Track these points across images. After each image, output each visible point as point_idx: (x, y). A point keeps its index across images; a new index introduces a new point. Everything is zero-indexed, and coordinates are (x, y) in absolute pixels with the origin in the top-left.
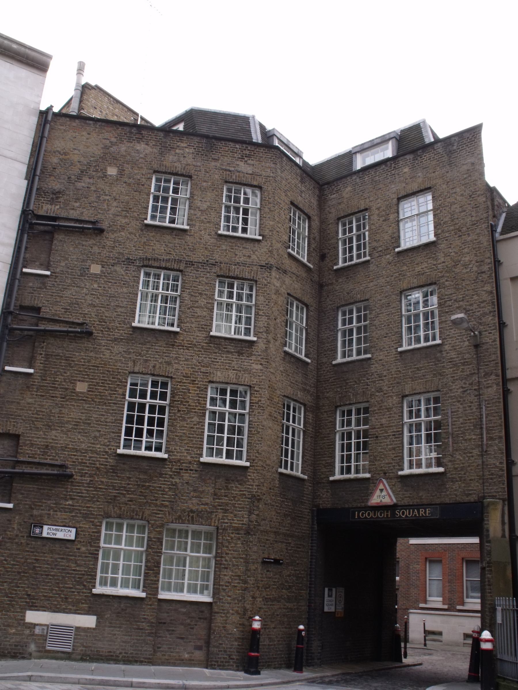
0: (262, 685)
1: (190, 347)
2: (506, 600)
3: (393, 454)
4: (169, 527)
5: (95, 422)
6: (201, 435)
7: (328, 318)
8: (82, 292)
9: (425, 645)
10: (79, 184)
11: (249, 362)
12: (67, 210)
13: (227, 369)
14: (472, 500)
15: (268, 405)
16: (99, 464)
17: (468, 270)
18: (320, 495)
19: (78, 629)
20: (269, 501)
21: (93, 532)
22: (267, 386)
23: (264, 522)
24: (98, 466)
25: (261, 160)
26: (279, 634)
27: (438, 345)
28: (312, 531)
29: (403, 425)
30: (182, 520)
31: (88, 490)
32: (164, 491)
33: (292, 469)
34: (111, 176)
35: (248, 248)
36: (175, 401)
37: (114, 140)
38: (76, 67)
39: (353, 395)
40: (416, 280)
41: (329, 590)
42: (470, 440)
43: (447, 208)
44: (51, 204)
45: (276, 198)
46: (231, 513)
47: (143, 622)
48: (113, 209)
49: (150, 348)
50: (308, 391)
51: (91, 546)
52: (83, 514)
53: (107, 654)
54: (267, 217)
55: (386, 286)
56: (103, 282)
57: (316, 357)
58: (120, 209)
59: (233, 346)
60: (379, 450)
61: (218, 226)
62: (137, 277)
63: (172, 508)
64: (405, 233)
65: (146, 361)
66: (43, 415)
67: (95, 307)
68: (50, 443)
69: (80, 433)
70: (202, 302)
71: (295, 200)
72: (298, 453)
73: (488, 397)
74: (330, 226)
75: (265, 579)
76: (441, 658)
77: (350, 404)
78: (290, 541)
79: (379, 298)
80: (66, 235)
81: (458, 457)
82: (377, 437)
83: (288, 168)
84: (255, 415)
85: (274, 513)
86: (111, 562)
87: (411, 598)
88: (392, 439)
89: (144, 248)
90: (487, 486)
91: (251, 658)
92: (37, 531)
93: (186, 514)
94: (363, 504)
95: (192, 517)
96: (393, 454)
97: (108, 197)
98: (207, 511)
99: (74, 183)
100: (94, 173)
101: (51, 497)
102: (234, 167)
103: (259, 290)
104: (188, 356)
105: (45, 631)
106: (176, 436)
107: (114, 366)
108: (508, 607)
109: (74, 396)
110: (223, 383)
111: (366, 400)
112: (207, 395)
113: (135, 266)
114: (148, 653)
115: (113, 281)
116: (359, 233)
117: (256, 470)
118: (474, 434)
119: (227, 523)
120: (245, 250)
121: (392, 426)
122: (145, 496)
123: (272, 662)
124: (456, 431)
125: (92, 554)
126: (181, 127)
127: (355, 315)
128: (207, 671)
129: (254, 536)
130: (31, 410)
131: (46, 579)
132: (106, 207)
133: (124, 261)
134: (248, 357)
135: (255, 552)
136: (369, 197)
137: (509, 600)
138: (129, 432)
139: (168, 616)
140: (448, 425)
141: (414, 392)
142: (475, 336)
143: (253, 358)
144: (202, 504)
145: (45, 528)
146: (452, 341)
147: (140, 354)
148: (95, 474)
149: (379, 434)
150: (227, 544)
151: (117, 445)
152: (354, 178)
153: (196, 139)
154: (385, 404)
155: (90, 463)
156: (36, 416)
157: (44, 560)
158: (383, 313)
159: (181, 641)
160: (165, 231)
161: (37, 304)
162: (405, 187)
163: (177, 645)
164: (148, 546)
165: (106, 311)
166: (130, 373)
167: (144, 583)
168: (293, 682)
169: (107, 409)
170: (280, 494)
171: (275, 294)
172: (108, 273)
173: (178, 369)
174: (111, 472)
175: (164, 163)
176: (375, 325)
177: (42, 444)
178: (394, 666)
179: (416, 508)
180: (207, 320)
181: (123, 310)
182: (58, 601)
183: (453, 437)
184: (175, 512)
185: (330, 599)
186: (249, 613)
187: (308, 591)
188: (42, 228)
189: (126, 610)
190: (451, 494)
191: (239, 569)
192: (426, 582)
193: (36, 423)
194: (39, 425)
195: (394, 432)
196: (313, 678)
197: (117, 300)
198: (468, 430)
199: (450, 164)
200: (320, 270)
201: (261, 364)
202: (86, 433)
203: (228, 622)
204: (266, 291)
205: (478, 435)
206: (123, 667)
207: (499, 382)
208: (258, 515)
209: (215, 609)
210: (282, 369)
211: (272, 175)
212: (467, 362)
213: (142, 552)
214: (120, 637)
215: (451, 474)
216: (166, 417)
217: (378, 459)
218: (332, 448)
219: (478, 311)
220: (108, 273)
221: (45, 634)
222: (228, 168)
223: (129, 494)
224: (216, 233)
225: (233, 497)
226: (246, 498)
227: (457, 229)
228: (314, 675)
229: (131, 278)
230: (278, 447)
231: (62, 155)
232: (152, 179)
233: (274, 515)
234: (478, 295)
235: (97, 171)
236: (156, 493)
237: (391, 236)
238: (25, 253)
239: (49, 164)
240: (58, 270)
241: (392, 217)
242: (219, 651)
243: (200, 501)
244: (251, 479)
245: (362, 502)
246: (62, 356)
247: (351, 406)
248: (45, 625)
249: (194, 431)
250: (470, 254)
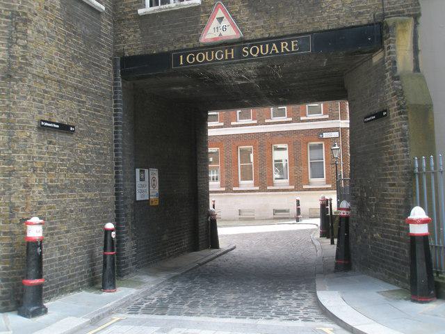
14: (365, 22)
18: (124, 37)
28: (115, 89)
78: (84, 99)
85: (55, 50)
94: (192, 44)
123: (67, 283)
129: (20, 83)
179: (274, 42)
185: (142, 183)
190: (329, 17)
208: (25, 47)
233: (56, 54)
245: (190, 41)
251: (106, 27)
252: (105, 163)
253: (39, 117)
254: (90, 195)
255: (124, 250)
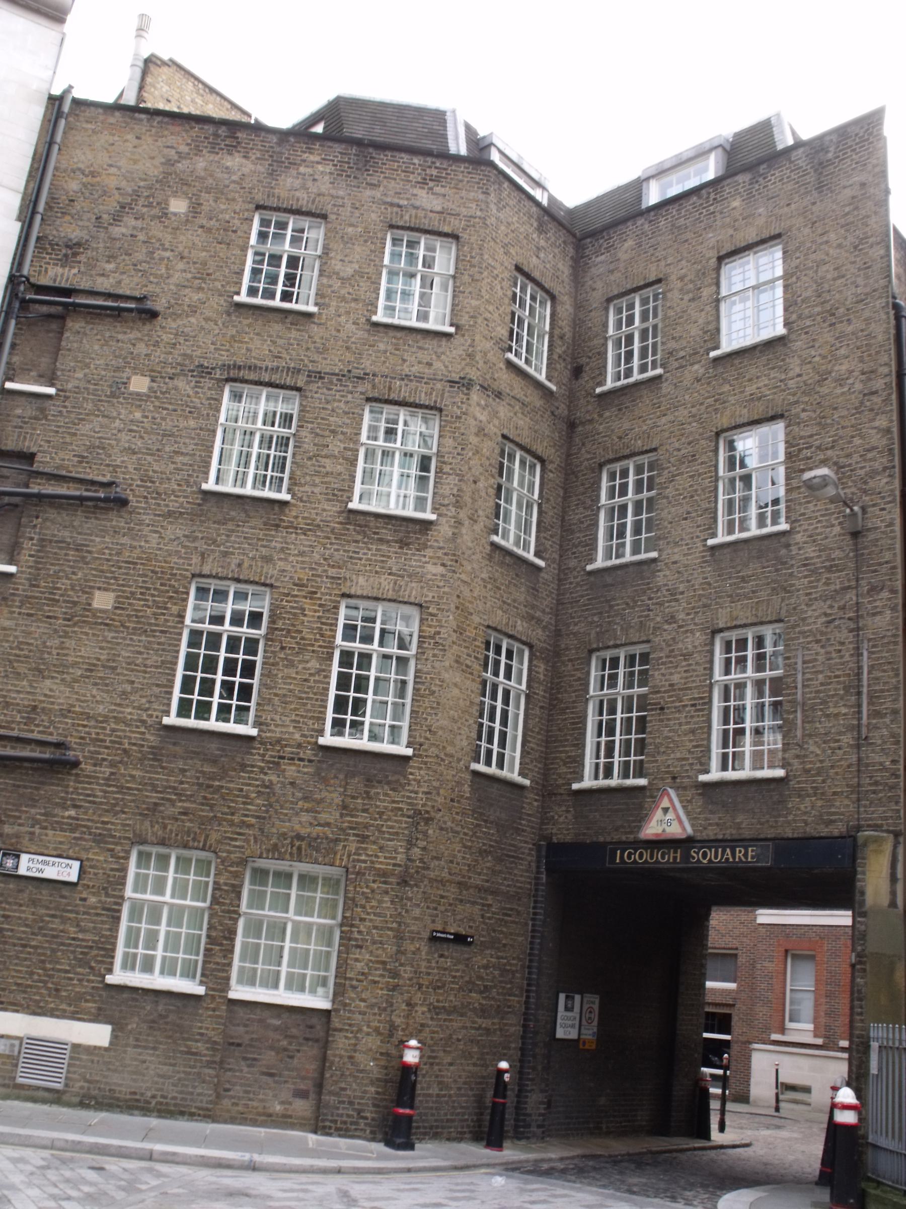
0: (409, 1170)
1: (310, 530)
2: (888, 1027)
3: (691, 741)
4: (256, 865)
5: (124, 665)
6: (322, 694)
7: (583, 484)
8: (113, 426)
9: (777, 1109)
10: (117, 229)
11: (420, 561)
12: (91, 276)
13: (377, 572)
14: (836, 833)
15: (453, 643)
16: (130, 744)
17: (846, 389)
19: (77, 1048)
20: (449, 824)
21: (112, 870)
22: (453, 606)
23: (437, 863)
24: (127, 746)
25: (460, 186)
26: (460, 1077)
27: (783, 533)
28: (536, 884)
29: (711, 686)
30: (280, 853)
31: (105, 792)
32: (247, 797)
33: (500, 765)
34: (175, 214)
35: (427, 349)
36: (276, 629)
37: (184, 149)
38: (135, 24)
39: (622, 629)
40: (746, 410)
41: (567, 997)
42: (837, 715)
43: (811, 273)
44: (62, 266)
45: (486, 257)
46: (374, 843)
47: (197, 1041)
48: (177, 275)
49: (233, 531)
50: (539, 621)
51: (107, 895)
52: (95, 835)
53: (128, 1097)
54: (467, 291)
55: (690, 423)
56: (151, 408)
57: (557, 557)
58: (189, 276)
59: (390, 530)
60: (666, 733)
61: (372, 307)
62: (215, 399)
63: (262, 830)
64: (730, 323)
65: (225, 554)
66: (30, 651)
67: (134, 453)
68: (41, 702)
69: (96, 684)
70: (336, 446)
71: (525, 263)
72: (515, 737)
73: (873, 634)
74: (593, 314)
75: (435, 971)
76: (795, 1135)
77: (616, 646)
78: (490, 902)
79: (677, 445)
80: (87, 323)
81: (812, 748)
82: (662, 709)
83: (511, 203)
84: (427, 660)
85: (458, 847)
86: (143, 926)
87: (756, 1022)
88: (689, 712)
89: (231, 346)
90: (865, 806)
91: (398, 1118)
92: (10, 863)
93: (288, 841)
95: (299, 848)
96: (691, 741)
97: (167, 254)
98: (327, 838)
99: (107, 228)
100: (145, 210)
101: (37, 801)
102: (408, 199)
103: (445, 426)
104: (304, 546)
105: (16, 1049)
106: (276, 695)
107: (166, 562)
108: (891, 1044)
109: (87, 616)
110: (368, 598)
111: (645, 638)
112: (337, 619)
113: (212, 379)
114: (205, 1099)
115: (170, 407)
116: (645, 325)
117: (426, 763)
118: (844, 705)
119: (365, 862)
120: (421, 352)
121: (690, 689)
122: (212, 806)
123: (443, 1127)
124: (810, 699)
125: (108, 910)
126: (319, 129)
127: (631, 479)
128: (312, 1139)
129: (415, 889)
130: (7, 641)
131: (22, 952)
132: (163, 271)
133: (193, 371)
134: (418, 550)
135: (416, 919)
136: (665, 258)
137: (894, 1028)
138: (187, 685)
139: (247, 1032)
140: (796, 688)
141: (734, 623)
142: (853, 514)
143: (429, 552)
144: (319, 825)
145: (24, 858)
146: (809, 525)
147: (214, 542)
148: (120, 762)
149: (667, 703)
150: (363, 902)
151: (165, 708)
152: (639, 223)
153: (338, 148)
154: (680, 645)
155: (111, 741)
156: (17, 652)
157: (20, 918)
158: (682, 474)
159: (270, 1080)
160: (271, 316)
161: (29, 447)
162: (732, 236)
163: (260, 1087)
164: (215, 901)
165: (155, 461)
166: (194, 576)
167: (203, 969)
168: (475, 1167)
169: (149, 642)
170: (474, 811)
171: (477, 435)
172: (162, 393)
173: (284, 571)
174: (150, 759)
175: (276, 191)
176: (668, 498)
177: (26, 703)
178: (691, 1146)
180: (343, 480)
181: (186, 459)
182: (41, 994)
183: (803, 711)
184: (267, 837)
185: (569, 1014)
186: (400, 1033)
187: (524, 999)
188: (45, 309)
189: (166, 1017)
191: (384, 949)
192: (784, 994)
193: (15, 664)
194: (22, 668)
195: (695, 699)
196: (520, 1162)
197: (176, 442)
198: (833, 696)
199: (820, 188)
200: (572, 397)
201: (443, 565)
202: (107, 685)
203: (358, 1047)
204: (459, 428)
205: (851, 706)
206: (154, 1122)
207: (896, 605)
208: (424, 849)
209: (336, 1022)
210: (485, 575)
211: (479, 213)
212: (836, 565)
213: (203, 910)
214: (153, 1067)
215: (799, 782)
216: (259, 659)
217: (662, 750)
218: (580, 728)
219: (862, 468)
220: (162, 393)
221: (16, 1053)
222: (396, 201)
223: (181, 801)
224: (368, 320)
225: (378, 813)
226: (403, 815)
227: (828, 311)
228: (532, 1156)
229: (204, 401)
230: (471, 722)
231: (87, 176)
232: (252, 220)
233: (459, 851)
234: (862, 437)
235: (150, 205)
236: (232, 801)
237: (702, 329)
238: (10, 354)
239: (62, 192)
240: (70, 386)
241: (706, 292)
242: (340, 1102)
243: (315, 818)
244: (415, 780)
245: (631, 833)
246: (69, 544)
247: (617, 650)
248: (17, 1038)
249: (309, 687)
250: (850, 359)
251: (531, 803)
252: (511, 983)
253: (432, 926)
254: (485, 1023)
255: (526, 1103)
